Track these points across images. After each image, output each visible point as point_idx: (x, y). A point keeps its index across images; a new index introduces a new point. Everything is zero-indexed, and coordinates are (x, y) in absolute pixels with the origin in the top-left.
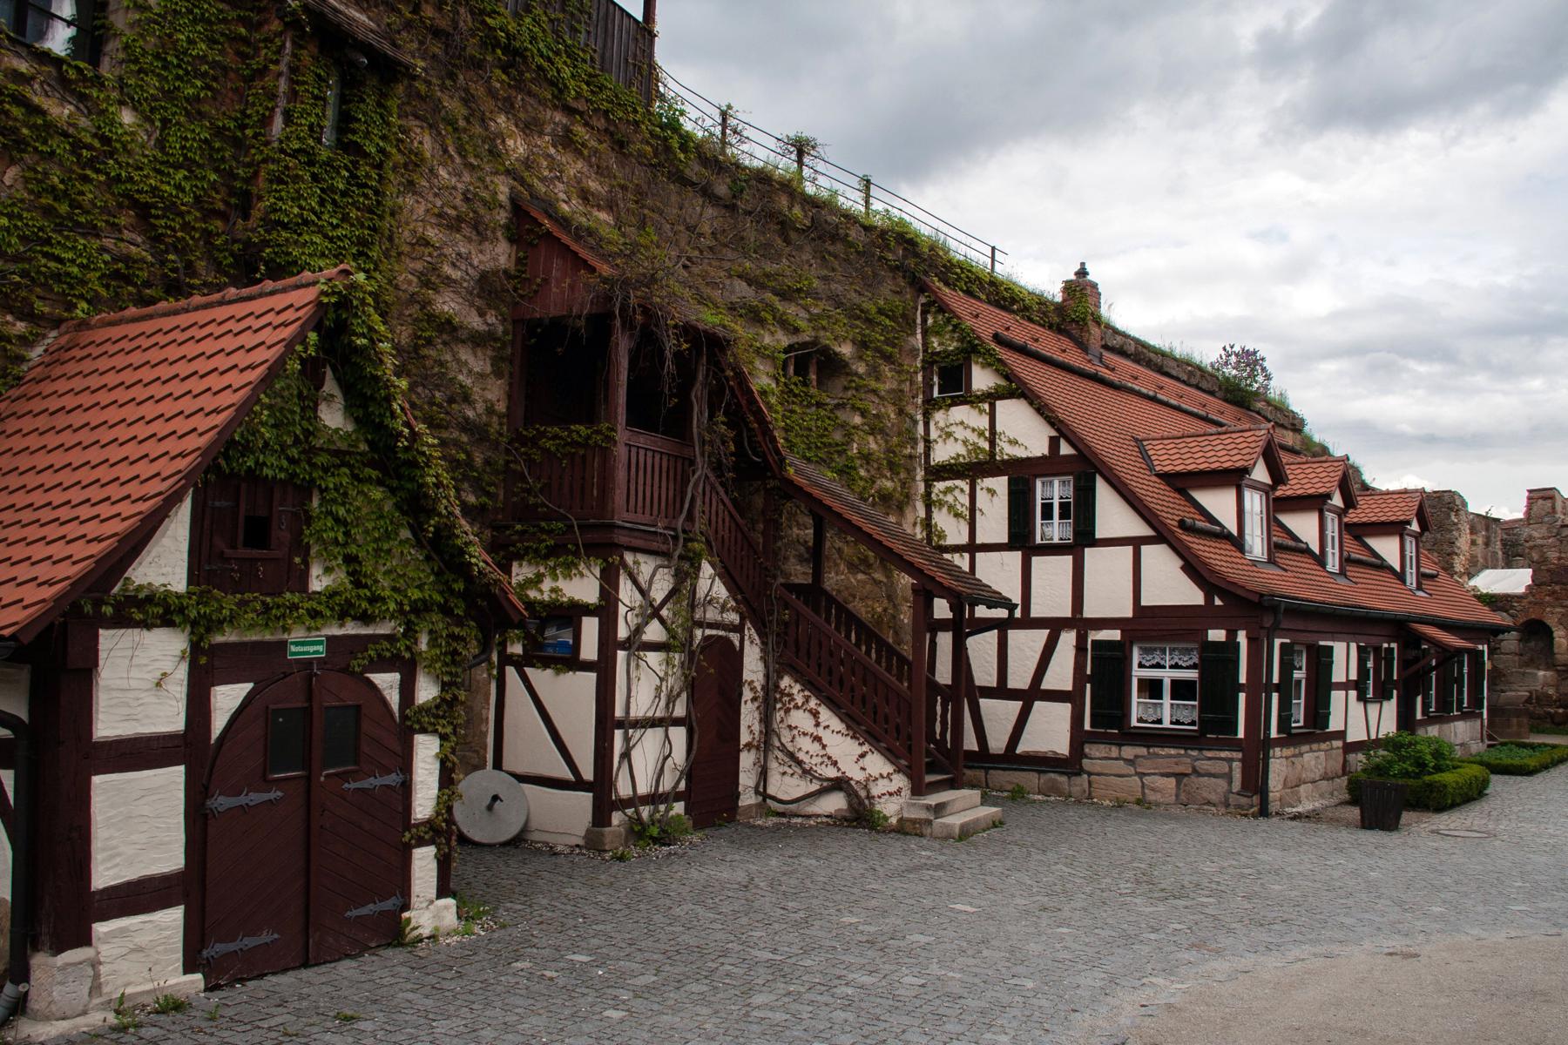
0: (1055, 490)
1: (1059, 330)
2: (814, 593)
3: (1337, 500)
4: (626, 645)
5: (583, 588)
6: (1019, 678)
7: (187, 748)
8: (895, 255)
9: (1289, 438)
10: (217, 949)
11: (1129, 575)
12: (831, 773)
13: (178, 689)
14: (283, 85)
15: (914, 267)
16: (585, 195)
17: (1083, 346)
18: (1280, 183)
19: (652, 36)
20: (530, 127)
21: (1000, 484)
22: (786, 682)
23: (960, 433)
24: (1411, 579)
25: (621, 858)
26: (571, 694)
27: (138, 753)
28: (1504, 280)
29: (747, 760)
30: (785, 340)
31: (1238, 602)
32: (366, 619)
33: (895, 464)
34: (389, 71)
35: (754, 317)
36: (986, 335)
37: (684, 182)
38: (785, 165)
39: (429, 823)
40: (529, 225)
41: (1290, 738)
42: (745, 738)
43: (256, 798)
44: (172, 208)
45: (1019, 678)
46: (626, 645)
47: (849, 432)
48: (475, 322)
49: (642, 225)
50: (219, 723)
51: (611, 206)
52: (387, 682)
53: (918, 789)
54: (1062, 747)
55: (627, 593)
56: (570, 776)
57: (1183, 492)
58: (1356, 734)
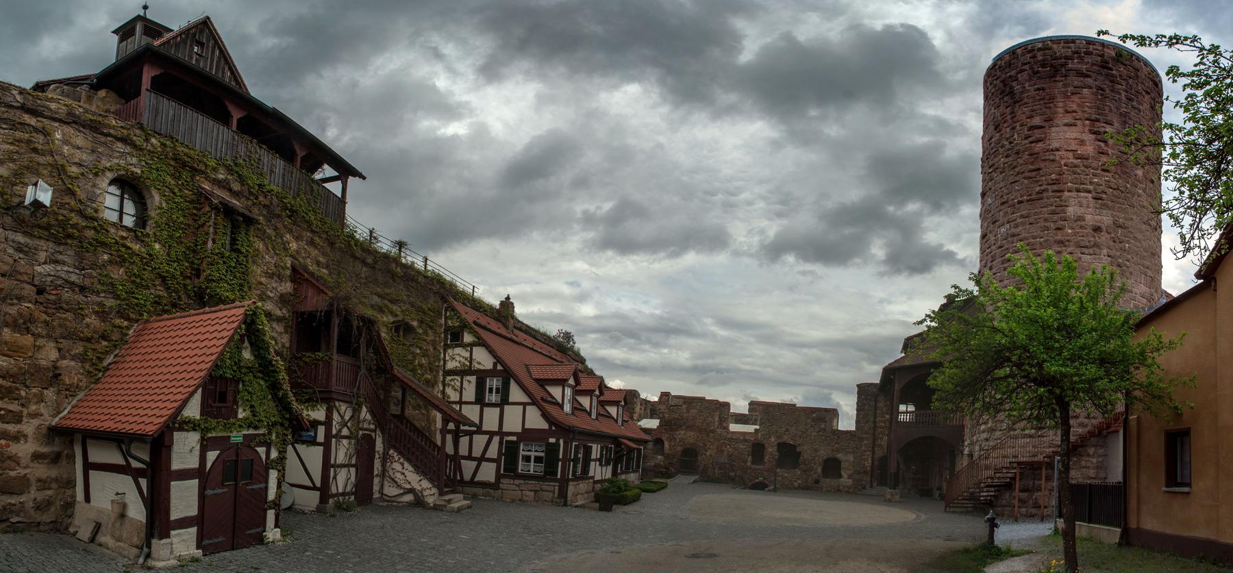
0: (495, 383)
1: (498, 320)
2: (401, 418)
3: (597, 393)
4: (336, 436)
5: (319, 414)
6: (477, 452)
7: (198, 472)
8: (436, 288)
9: (580, 366)
10: (206, 542)
11: (519, 416)
12: (408, 486)
13: (197, 452)
14: (211, 230)
15: (442, 292)
16: (318, 263)
17: (507, 327)
18: (580, 265)
19: (345, 203)
20: (298, 238)
21: (473, 379)
22: (391, 452)
23: (458, 358)
24: (620, 422)
25: (333, 516)
26: (313, 457)
27: (184, 475)
28: (657, 312)
29: (376, 480)
30: (392, 319)
31: (559, 428)
32: (256, 428)
33: (432, 369)
34: (249, 221)
35: (381, 310)
36: (471, 321)
37: (355, 258)
38: (394, 251)
39: (273, 501)
40: (297, 275)
41: (576, 478)
42: (376, 472)
43: (220, 491)
44: (173, 276)
45: (477, 452)
46: (336, 436)
47: (414, 355)
48: (279, 313)
49: (339, 274)
50: (209, 465)
51: (327, 267)
52: (261, 450)
53: (441, 494)
54: (492, 479)
55: (336, 416)
56: (310, 484)
57: (542, 386)
58: (598, 478)
